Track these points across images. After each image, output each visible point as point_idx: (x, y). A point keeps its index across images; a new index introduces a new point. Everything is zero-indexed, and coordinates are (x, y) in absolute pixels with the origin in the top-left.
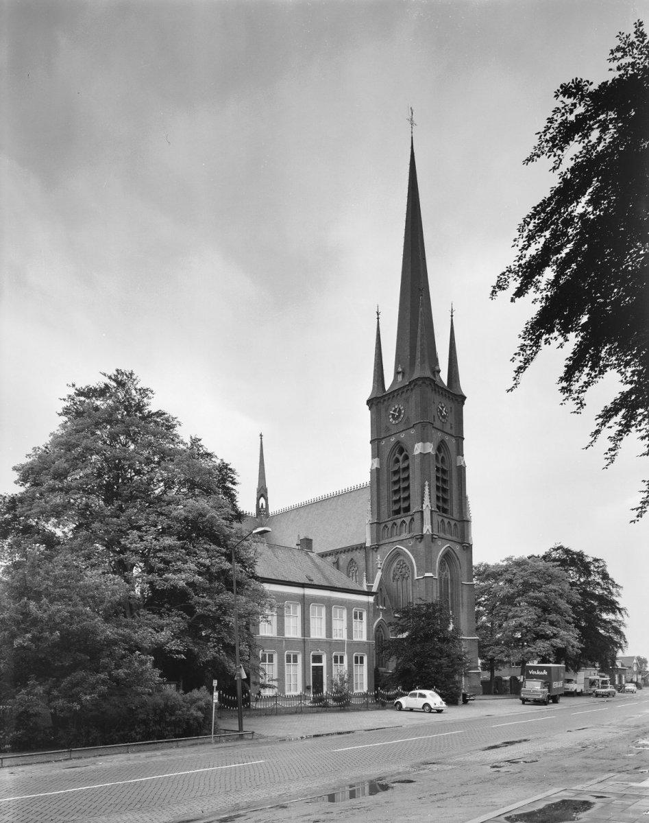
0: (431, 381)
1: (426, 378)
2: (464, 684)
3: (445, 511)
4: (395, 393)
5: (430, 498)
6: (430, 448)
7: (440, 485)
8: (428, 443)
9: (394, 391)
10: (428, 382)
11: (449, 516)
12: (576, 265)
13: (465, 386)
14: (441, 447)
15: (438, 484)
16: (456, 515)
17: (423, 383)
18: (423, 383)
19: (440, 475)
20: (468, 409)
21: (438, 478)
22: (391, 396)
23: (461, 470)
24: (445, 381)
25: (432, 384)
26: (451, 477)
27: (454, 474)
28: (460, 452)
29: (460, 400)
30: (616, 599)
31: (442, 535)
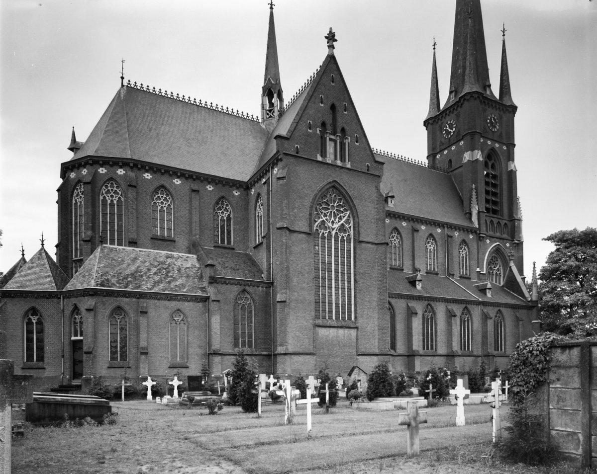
0: (482, 98)
1: (474, 92)
2: (36, 405)
3: (495, 212)
4: (449, 110)
5: (477, 201)
6: (478, 155)
7: (490, 207)
8: (476, 151)
9: (451, 107)
10: (476, 96)
11: (499, 217)
12: (561, 312)
13: (516, 98)
14: (491, 155)
15: (487, 197)
16: (506, 216)
17: (471, 97)
18: (471, 97)
19: (490, 189)
20: (516, 149)
21: (487, 192)
22: (448, 112)
23: (512, 176)
24: (497, 94)
25: (481, 97)
26: (501, 199)
27: (505, 177)
28: (510, 157)
29: (510, 110)
30: (75, 276)
31: (491, 233)
